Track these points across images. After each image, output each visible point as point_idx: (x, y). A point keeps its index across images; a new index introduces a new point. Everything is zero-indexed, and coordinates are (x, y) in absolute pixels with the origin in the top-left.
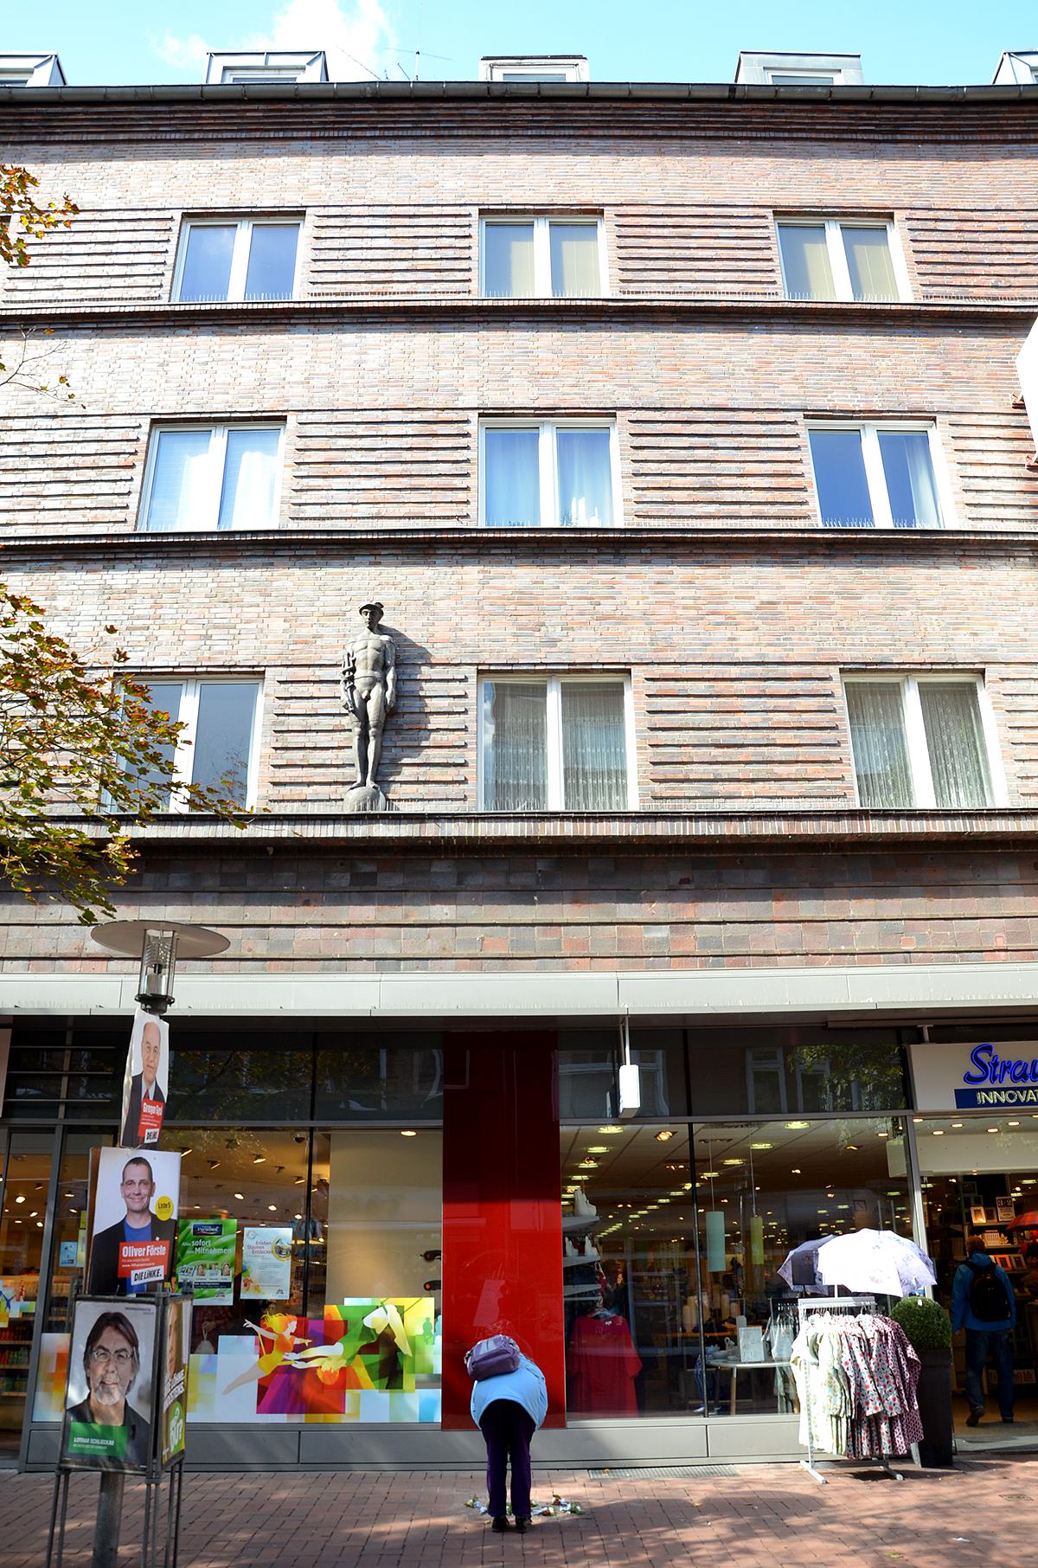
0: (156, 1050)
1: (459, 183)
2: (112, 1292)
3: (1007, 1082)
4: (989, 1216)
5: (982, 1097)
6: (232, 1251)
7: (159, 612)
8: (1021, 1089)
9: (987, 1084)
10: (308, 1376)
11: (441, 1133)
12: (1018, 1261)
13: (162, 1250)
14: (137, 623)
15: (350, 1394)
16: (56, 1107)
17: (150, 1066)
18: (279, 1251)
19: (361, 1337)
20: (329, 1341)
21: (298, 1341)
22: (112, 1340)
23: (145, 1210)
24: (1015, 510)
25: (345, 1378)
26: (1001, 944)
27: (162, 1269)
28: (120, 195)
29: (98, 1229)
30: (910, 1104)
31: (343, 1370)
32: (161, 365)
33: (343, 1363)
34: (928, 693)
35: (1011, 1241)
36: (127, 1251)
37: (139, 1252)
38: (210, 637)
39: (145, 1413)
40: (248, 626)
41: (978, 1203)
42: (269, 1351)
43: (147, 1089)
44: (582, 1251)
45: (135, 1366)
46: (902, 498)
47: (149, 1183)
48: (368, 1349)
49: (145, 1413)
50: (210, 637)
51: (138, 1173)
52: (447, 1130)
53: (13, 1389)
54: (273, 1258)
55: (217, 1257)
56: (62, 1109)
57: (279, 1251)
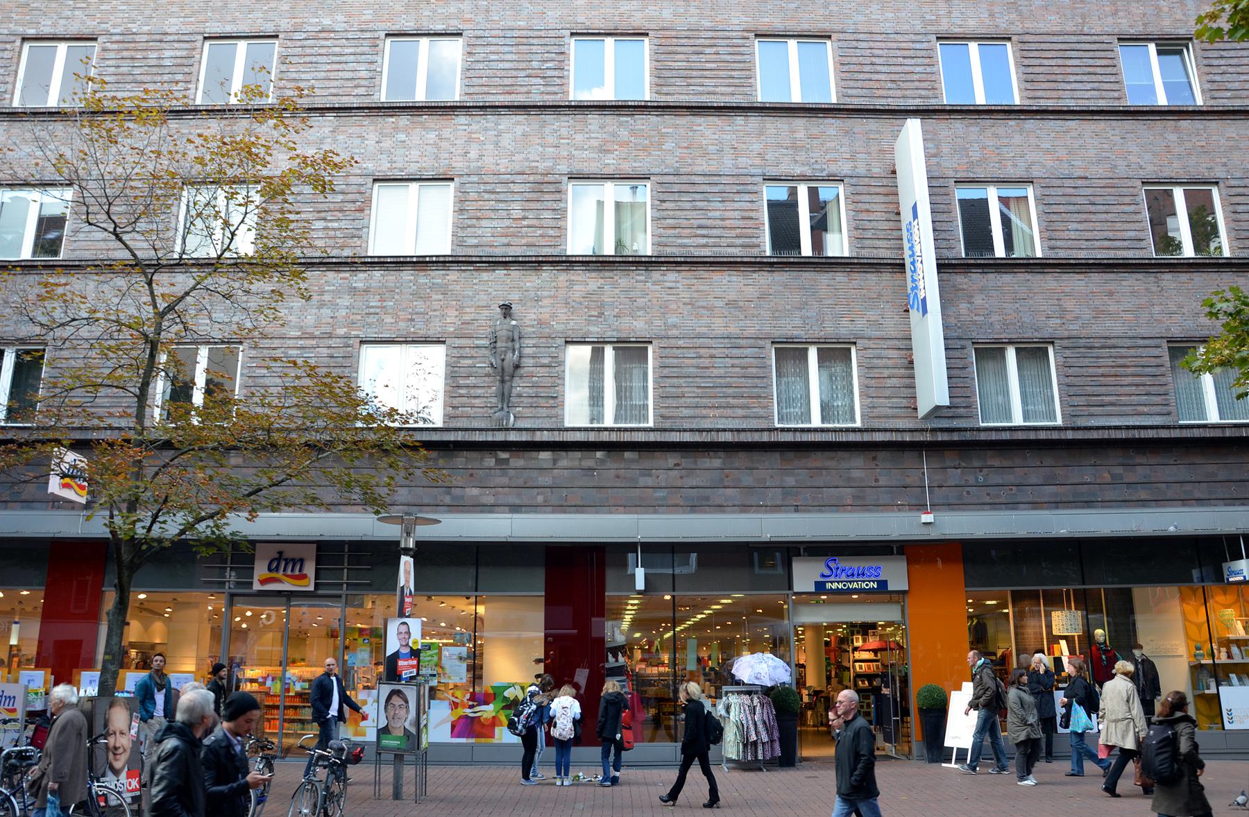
0: (409, 572)
1: (559, 13)
2: (395, 680)
3: (844, 578)
4: (864, 641)
5: (828, 586)
6: (436, 658)
7: (384, 304)
8: (850, 582)
9: (832, 579)
10: (476, 720)
11: (543, 599)
12: (878, 667)
13: (415, 662)
14: (372, 310)
15: (497, 730)
16: (342, 584)
17: (407, 581)
18: (461, 658)
19: (503, 701)
20: (487, 703)
21: (471, 703)
22: (396, 700)
23: (407, 645)
24: (885, 242)
25: (494, 722)
26: (849, 502)
27: (415, 670)
28: (345, 20)
29: (388, 653)
30: (790, 587)
31: (494, 717)
32: (377, 142)
33: (494, 714)
34: (823, 356)
35: (876, 655)
36: (401, 663)
37: (405, 663)
38: (413, 320)
39: (413, 730)
40: (435, 313)
41: (858, 633)
42: (456, 708)
43: (407, 591)
44: (617, 661)
45: (408, 711)
46: (818, 244)
47: (409, 633)
48: (505, 708)
49: (413, 730)
50: (413, 320)
51: (403, 629)
52: (547, 597)
53: (303, 729)
54: (458, 662)
55: (429, 661)
56: (345, 586)
57: (461, 658)
